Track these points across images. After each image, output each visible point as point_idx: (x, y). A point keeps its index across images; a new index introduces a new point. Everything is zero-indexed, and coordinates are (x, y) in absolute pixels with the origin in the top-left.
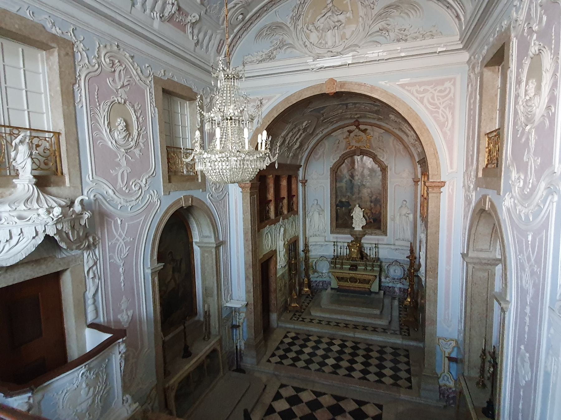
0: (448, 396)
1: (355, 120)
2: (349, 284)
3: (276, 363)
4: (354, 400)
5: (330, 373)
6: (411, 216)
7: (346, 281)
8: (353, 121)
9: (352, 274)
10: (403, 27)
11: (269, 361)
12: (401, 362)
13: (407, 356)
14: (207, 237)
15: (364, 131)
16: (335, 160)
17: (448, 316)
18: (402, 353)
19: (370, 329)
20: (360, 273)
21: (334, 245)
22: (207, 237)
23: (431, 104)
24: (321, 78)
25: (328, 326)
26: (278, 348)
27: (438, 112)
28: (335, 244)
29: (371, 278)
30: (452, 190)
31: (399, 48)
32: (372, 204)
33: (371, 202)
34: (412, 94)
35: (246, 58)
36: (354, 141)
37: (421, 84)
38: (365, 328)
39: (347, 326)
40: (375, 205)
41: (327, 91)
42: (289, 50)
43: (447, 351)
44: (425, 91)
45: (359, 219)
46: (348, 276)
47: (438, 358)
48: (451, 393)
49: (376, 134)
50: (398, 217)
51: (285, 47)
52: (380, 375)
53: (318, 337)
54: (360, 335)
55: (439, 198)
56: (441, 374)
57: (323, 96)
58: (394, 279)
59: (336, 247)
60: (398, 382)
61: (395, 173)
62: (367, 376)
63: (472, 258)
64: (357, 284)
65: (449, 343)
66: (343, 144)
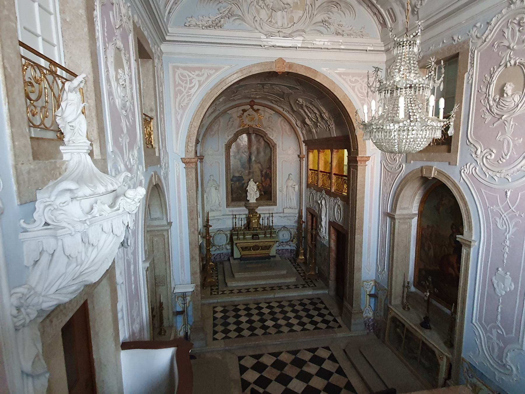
1: (250, 100)
3: (223, 339)
4: (306, 350)
5: (276, 333)
6: (297, 187)
9: (255, 242)
10: (341, 23)
11: (215, 339)
13: (322, 303)
14: (156, 219)
15: (257, 111)
16: (230, 137)
18: (241, 307)
19: (236, 291)
20: (262, 241)
21: (233, 218)
22: (156, 219)
24: (273, 55)
25: (265, 291)
26: (215, 325)
27: (364, 100)
28: (234, 217)
29: (272, 244)
30: (374, 163)
31: (341, 41)
33: (262, 176)
34: (347, 82)
35: (189, 20)
36: (247, 120)
37: (354, 75)
38: (280, 288)
39: (264, 289)
40: (265, 179)
42: (238, 22)
43: (368, 290)
44: (357, 81)
45: (253, 192)
46: (252, 245)
47: (362, 296)
49: (267, 115)
51: (235, 18)
52: (226, 331)
53: (244, 305)
58: (283, 242)
59: (234, 219)
62: (255, 332)
63: (400, 215)
64: (258, 251)
65: (369, 283)
66: (237, 122)
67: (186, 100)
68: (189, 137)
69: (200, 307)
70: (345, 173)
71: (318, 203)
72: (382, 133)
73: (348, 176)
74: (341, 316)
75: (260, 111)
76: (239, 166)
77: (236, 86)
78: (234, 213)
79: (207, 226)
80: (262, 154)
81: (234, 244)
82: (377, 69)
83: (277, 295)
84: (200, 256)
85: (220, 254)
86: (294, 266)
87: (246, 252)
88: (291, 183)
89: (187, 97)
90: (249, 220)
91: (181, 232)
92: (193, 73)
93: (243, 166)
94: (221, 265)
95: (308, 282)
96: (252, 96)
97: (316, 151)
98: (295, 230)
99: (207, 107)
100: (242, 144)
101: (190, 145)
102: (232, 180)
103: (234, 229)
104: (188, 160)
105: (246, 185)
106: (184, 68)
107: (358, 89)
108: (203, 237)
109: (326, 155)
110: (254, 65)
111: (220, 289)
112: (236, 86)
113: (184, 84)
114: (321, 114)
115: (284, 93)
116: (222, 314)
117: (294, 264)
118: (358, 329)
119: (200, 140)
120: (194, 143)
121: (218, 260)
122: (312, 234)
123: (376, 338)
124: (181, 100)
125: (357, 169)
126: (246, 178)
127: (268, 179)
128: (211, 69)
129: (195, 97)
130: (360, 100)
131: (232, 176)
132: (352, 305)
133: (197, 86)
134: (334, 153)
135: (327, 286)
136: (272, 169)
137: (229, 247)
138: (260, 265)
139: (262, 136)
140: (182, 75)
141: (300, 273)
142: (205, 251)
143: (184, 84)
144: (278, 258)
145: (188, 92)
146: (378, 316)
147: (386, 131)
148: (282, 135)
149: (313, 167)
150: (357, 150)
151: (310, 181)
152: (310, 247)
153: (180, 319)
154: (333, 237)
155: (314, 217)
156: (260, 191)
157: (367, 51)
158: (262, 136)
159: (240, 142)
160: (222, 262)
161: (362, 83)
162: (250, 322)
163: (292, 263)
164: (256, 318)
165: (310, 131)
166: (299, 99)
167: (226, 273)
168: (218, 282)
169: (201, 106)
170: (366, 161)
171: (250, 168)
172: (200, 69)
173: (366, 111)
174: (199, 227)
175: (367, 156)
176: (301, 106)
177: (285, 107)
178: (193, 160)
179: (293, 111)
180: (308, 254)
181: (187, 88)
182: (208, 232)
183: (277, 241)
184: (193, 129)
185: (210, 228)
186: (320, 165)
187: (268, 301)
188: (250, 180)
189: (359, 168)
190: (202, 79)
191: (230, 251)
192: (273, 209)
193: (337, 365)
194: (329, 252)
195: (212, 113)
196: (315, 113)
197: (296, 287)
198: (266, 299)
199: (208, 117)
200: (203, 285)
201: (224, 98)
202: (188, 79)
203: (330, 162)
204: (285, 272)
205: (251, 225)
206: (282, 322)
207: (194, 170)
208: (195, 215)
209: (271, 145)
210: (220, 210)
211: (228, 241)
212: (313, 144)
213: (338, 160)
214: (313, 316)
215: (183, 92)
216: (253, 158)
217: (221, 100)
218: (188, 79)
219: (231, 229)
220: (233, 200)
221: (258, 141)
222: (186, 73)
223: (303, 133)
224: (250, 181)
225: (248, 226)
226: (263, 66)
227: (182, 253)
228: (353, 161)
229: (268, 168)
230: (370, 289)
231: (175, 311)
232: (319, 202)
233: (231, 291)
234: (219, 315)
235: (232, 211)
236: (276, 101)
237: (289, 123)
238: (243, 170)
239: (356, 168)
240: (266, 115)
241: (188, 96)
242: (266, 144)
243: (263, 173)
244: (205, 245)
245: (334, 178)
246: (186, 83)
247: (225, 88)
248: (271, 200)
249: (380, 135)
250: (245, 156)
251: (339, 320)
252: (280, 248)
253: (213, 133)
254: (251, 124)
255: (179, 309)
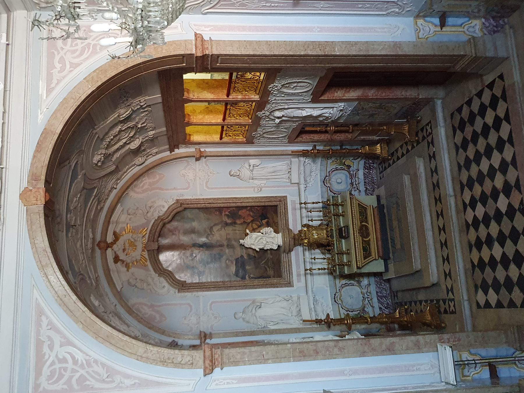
0: (496, 27)
1: (97, 248)
2: (373, 237)
5: (520, 192)
6: (253, 161)
7: (368, 243)
8: (98, 252)
12: (489, 234)
13: (460, 110)
15: (117, 237)
17: (384, 28)
20: (350, 220)
23: (81, 54)
27: (95, 45)
28: (309, 272)
30: (206, 26)
32: (238, 222)
33: (235, 223)
36: (133, 254)
37: (51, 66)
40: (240, 217)
41: (42, 202)
43: (433, 28)
44: (62, 61)
45: (264, 239)
46: (359, 239)
47: (445, 39)
48: (490, 24)
49: (124, 218)
50: (256, 182)
54: (449, 187)
55: (218, 42)
56: (470, 35)
57: (50, 211)
58: (352, 184)
59: (314, 271)
60: (499, 96)
61: (187, 189)
64: (370, 226)
65: (421, 27)
67: (96, 368)
68: (164, 362)
69: (480, 334)
70: (226, 76)
71: (280, 122)
72: (150, 11)
73: (231, 71)
74: (481, 76)
75: (118, 231)
76: (217, 265)
77: (70, 276)
78: (302, 272)
79: (328, 323)
80: (195, 224)
81: (359, 271)
82: (36, 23)
83: (450, 191)
84: (383, 336)
85: (380, 298)
86: (394, 162)
87: (373, 250)
88: (246, 172)
89: (92, 367)
90: (313, 245)
91: (342, 373)
92: (47, 357)
93: (217, 258)
94: (399, 295)
95: (423, 136)
96: (90, 245)
97: (188, 129)
98: (330, 161)
99: (109, 329)
100: (178, 261)
101: (179, 359)
102: (243, 278)
103: (331, 272)
104: (208, 362)
105: (251, 252)
106: (38, 373)
107: (75, 58)
108: (349, 329)
109: (194, 111)
110: (33, 244)
111: (445, 296)
112: (70, 276)
113: (67, 375)
114: (121, 122)
115: (84, 188)
116: (491, 291)
117: (391, 162)
118: (504, 45)
119: (170, 340)
120: (177, 351)
121: (390, 301)
122: (336, 132)
123: (516, 14)
124: (97, 380)
125: (218, 56)
126: (239, 252)
127: (240, 213)
128: (39, 324)
129: (91, 353)
130: (94, 52)
131: (234, 278)
132: (463, 56)
133: (71, 349)
134: (191, 96)
135: (429, 102)
136: (222, 205)
137: (365, 281)
138: (395, 223)
139: (164, 225)
140: (50, 377)
141: (408, 151)
142: (375, 327)
143: (67, 375)
144: (382, 191)
145: (82, 366)
146: (479, 11)
147: (146, 4)
148: (161, 189)
149: (216, 133)
150: (183, 56)
151: (241, 138)
152: (359, 135)
153: (504, 372)
154: (339, 94)
155: (304, 129)
156: (260, 226)
157: (8, 45)
158: (164, 225)
159: (174, 265)
160: (394, 294)
161: (64, 51)
162: (502, 239)
163: (389, 165)
164: (494, 229)
165: (153, 141)
166: (95, 161)
167: (414, 284)
168: (432, 301)
169: (107, 340)
170: (203, 40)
171: (221, 246)
172: (39, 344)
173: (110, 41)
174: (330, 337)
175: (193, 38)
176: (108, 157)
177: (109, 187)
178: (208, 353)
179: (117, 170)
180: (370, 138)
181: (74, 367)
182: (340, 321)
183: (351, 194)
184: (150, 355)
185: (332, 316)
186: (213, 121)
187: (461, 207)
188: (242, 245)
189: (215, 52)
190: (57, 339)
191: (372, 279)
192: (293, 202)
193: (497, 79)
194: (367, 100)
195: (120, 318)
196: (120, 131)
197: (433, 157)
198: (458, 212)
199: (128, 326)
200: (438, 328)
201: (92, 298)
202: (57, 366)
203: (206, 104)
204: (406, 179)
205: (324, 241)
206: (499, 182)
207: (227, 351)
208: (311, 347)
209: (179, 209)
210: (299, 298)
211: (355, 283)
212: (176, 134)
213: (203, 89)
214: (485, 124)
215: (82, 375)
216: (203, 240)
217: (96, 303)
218: (57, 366)
219: (331, 277)
220: (278, 274)
221: (172, 232)
222: (46, 371)
223: (157, 153)
224: (242, 243)
225: (324, 246)
226: (34, 227)
227: (381, 370)
228: (204, 63)
229: (221, 213)
230: (430, 25)
231: (488, 382)
232: (277, 121)
233: (448, 275)
234: (492, 297)
235: (299, 275)
236: (99, 202)
237: (128, 188)
238: (224, 257)
239: (216, 57)
240: (122, 219)
241: (89, 365)
242: (177, 218)
243: (229, 221)
244: (363, 326)
245: (235, 96)
246: (65, 369)
247: (74, 297)
248: (276, 206)
249: (155, 13)
250: (199, 255)
251: (488, 79)
252: (362, 188)
253: (157, 316)
254: (140, 247)
255: (486, 374)
